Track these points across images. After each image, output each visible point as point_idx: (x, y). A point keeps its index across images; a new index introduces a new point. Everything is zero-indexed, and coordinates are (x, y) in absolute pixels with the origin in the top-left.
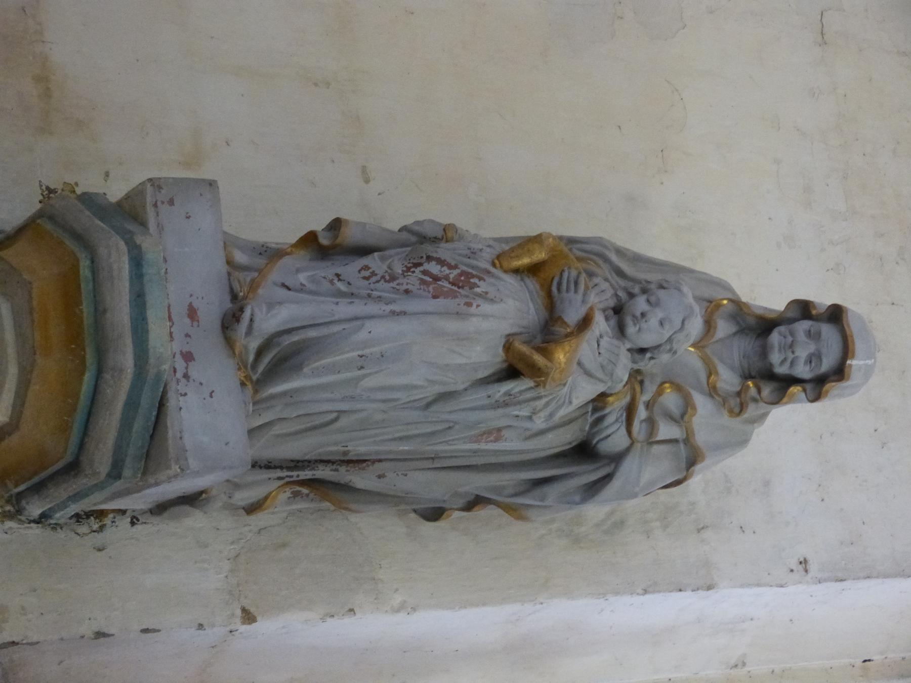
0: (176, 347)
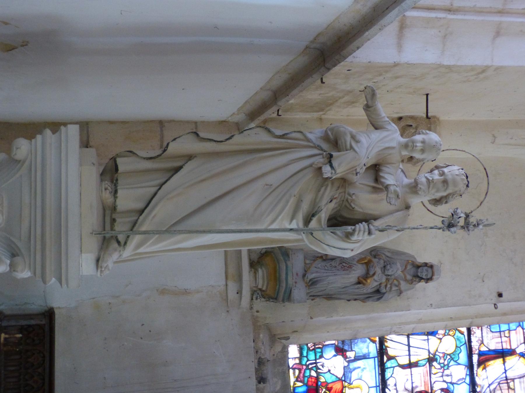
0: (294, 281)
